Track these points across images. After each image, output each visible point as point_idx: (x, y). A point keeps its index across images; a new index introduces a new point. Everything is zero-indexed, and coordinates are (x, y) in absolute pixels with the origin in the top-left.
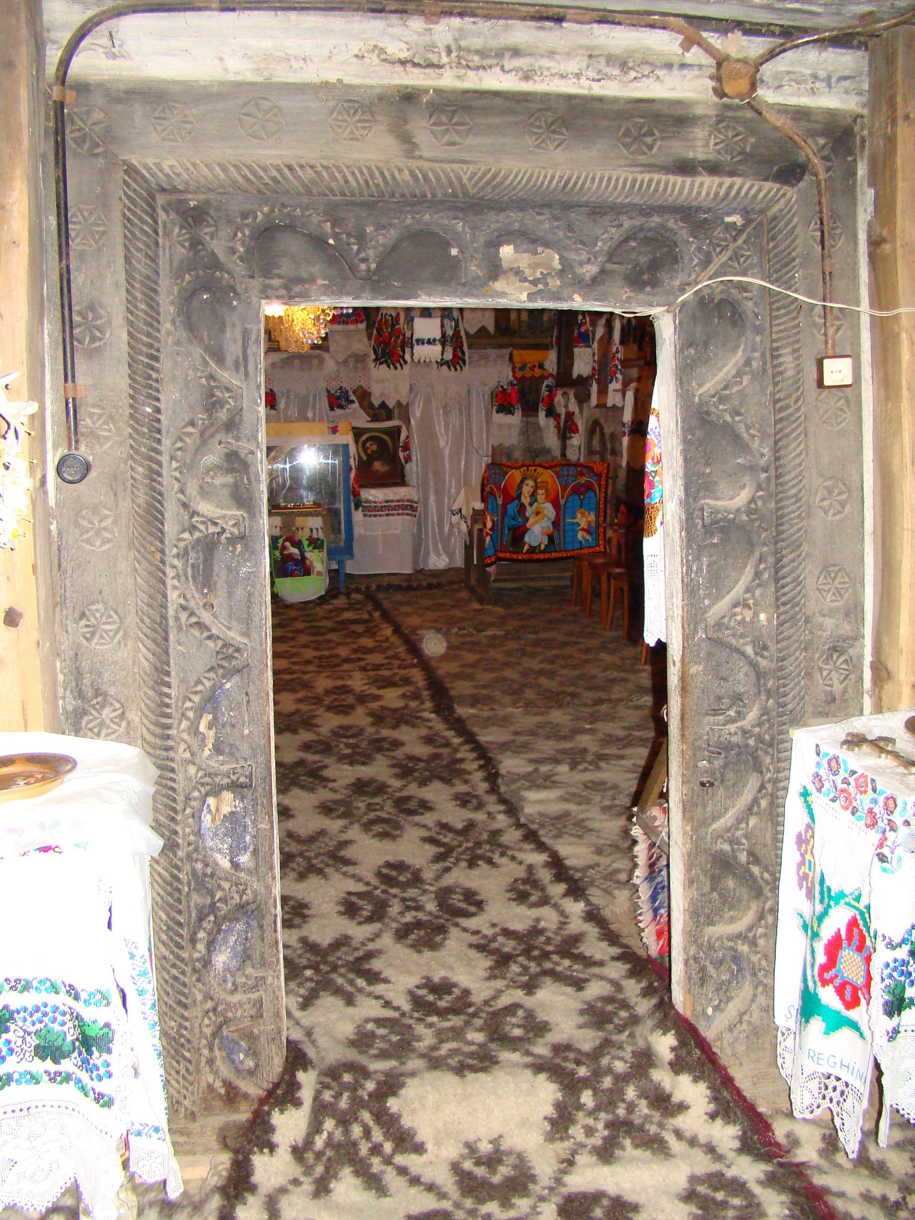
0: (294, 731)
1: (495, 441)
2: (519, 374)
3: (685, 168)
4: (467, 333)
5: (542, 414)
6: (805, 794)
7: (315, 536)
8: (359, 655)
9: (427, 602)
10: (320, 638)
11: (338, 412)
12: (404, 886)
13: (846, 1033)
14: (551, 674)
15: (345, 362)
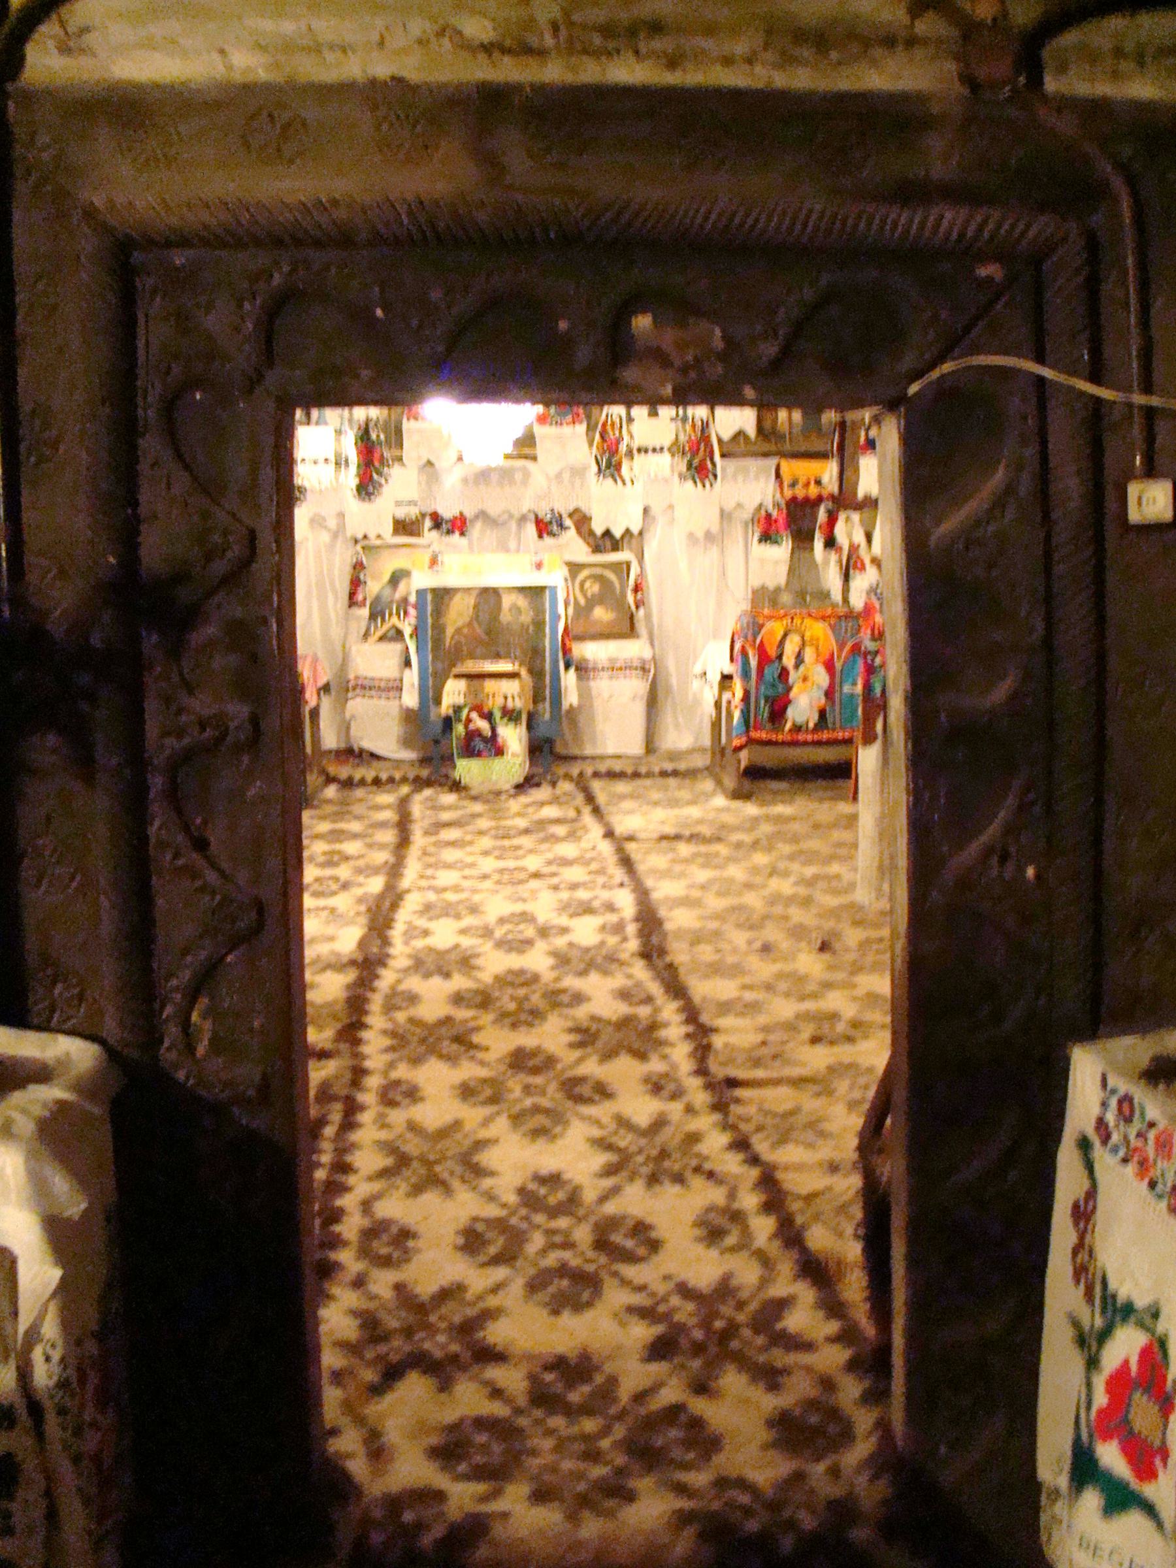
0: (447, 975)
1: (756, 583)
2: (788, 493)
3: (911, 193)
4: (720, 440)
5: (819, 544)
6: (1084, 1145)
7: (510, 704)
8: (553, 868)
9: (655, 795)
10: (506, 843)
11: (548, 540)
12: (554, 1212)
13: (1134, 1520)
14: (807, 902)
15: (559, 476)
